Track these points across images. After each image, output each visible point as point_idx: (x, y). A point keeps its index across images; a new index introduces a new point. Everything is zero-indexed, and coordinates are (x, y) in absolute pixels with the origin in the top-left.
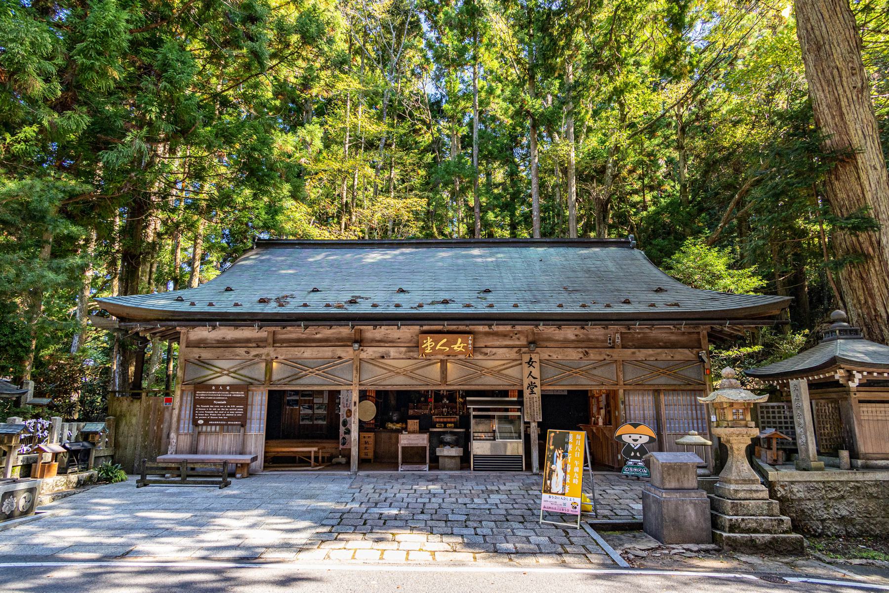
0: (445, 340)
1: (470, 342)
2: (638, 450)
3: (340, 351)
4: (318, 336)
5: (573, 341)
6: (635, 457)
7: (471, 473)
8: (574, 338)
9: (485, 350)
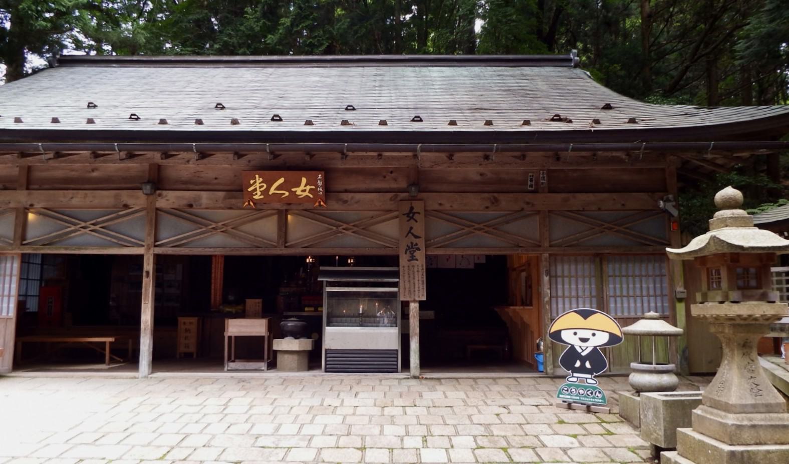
0: (282, 180)
1: (320, 183)
2: (589, 357)
3: (125, 197)
4: (95, 174)
5: (476, 183)
6: (582, 370)
7: (318, 375)
8: (478, 178)
9: (344, 196)
